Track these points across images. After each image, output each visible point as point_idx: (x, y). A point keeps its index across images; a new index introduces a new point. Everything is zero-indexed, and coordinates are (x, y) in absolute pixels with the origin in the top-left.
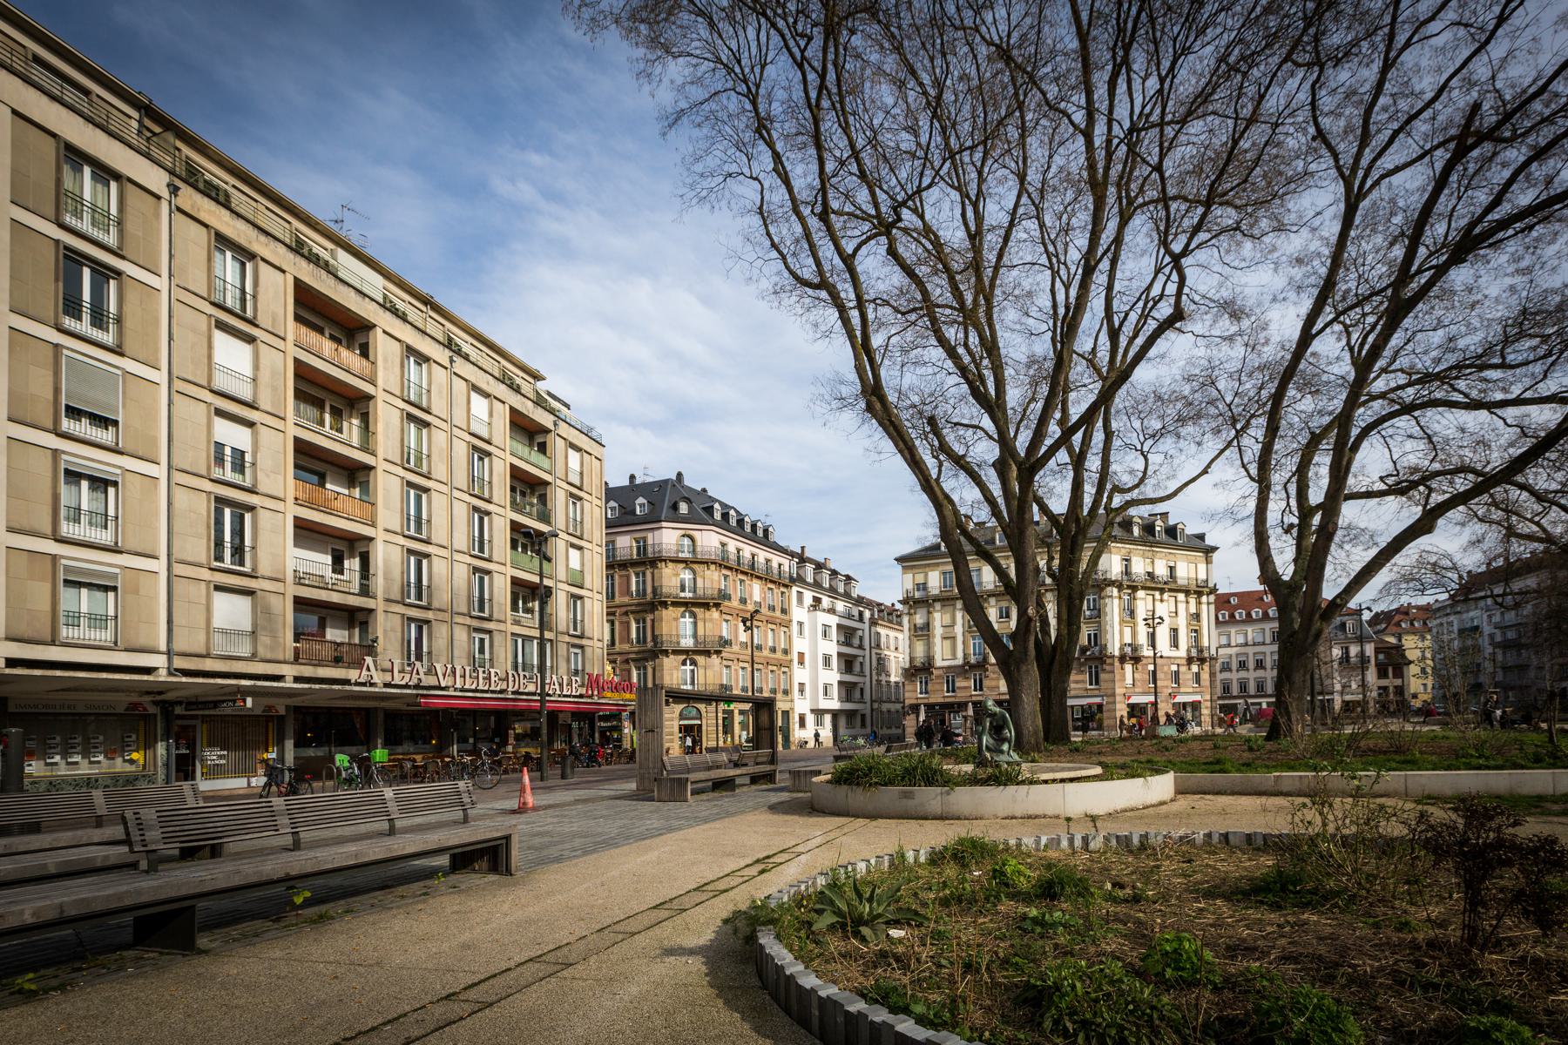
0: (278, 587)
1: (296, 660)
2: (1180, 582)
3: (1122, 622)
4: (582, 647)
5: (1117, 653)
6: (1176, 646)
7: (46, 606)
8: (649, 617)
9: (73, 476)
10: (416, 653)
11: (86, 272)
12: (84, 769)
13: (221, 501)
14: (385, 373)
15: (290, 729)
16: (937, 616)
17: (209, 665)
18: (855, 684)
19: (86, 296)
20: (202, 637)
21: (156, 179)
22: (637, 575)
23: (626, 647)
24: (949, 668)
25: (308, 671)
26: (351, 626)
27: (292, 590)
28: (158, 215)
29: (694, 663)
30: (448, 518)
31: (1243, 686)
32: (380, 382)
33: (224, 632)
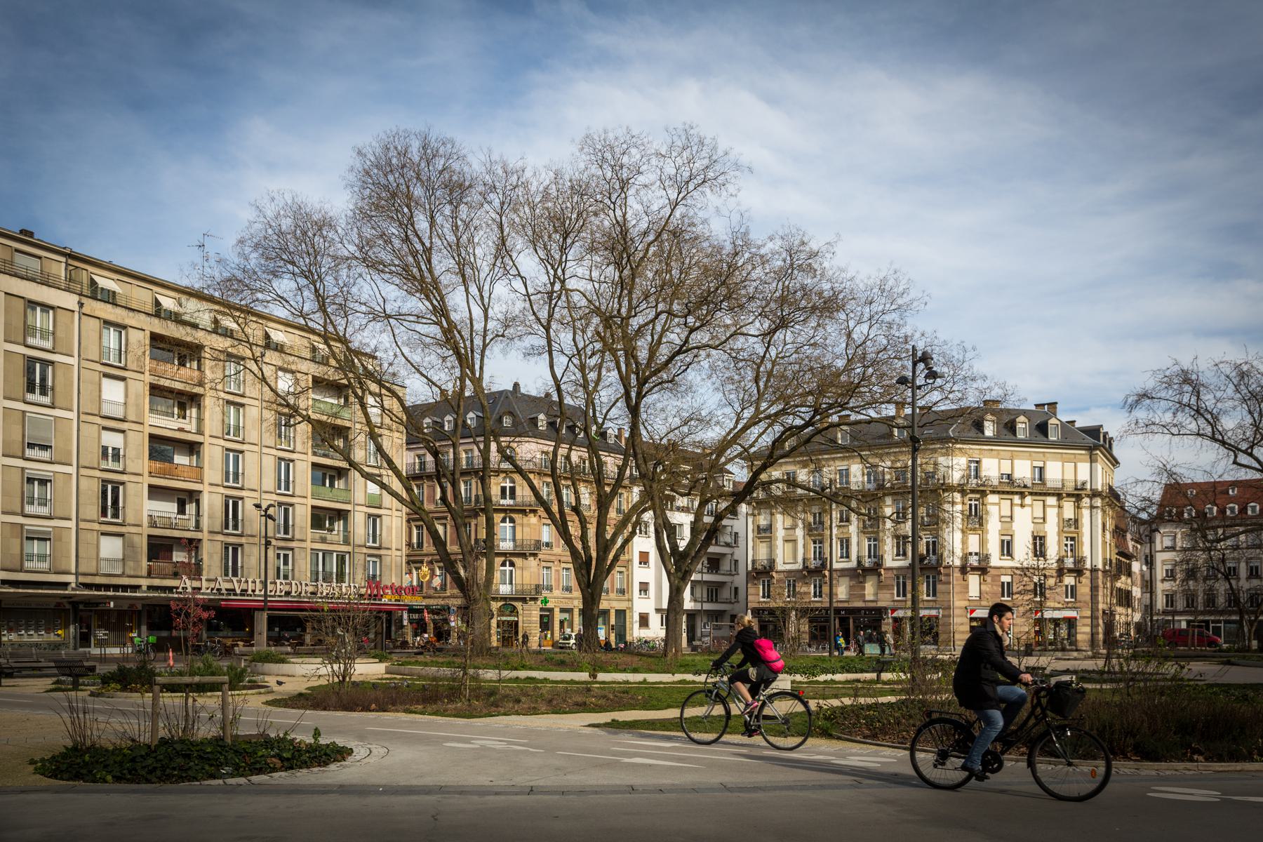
1: (149, 575)
2: (1049, 484)
4: (380, 556)
5: (958, 563)
7: (18, 551)
10: (232, 568)
12: (36, 639)
15: (144, 619)
16: (779, 517)
17: (98, 580)
18: (722, 584)
20: (94, 563)
22: (466, 483)
24: (790, 572)
25: (157, 582)
28: (73, 322)
29: (512, 564)
31: (1211, 599)
33: (107, 560)
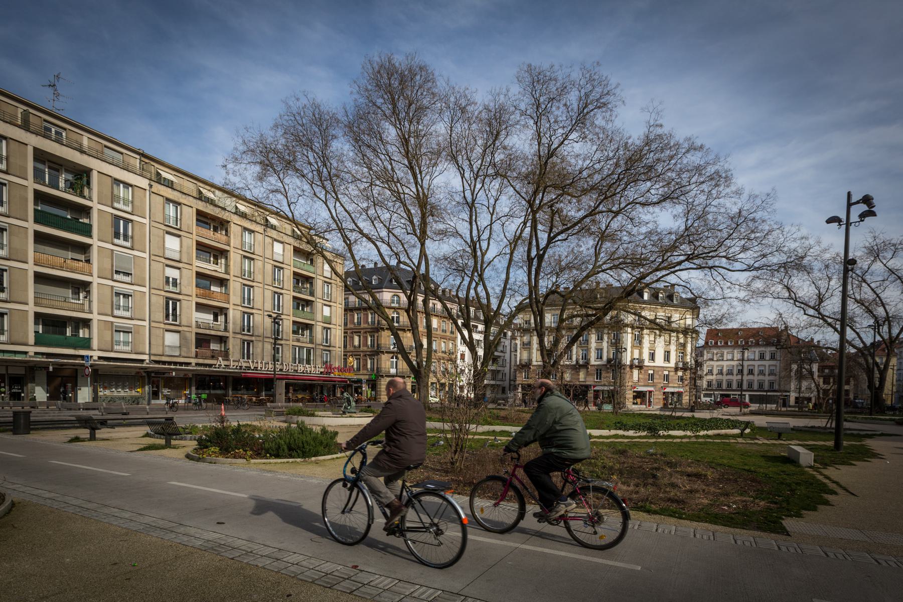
0: (189, 329)
1: (196, 357)
3: (633, 347)
5: (628, 363)
6: (668, 361)
7: (109, 339)
8: (376, 335)
9: (118, 294)
11: (122, 222)
12: (122, 394)
13: (168, 299)
14: (236, 239)
15: (194, 383)
18: (498, 371)
19: (122, 231)
21: (144, 183)
23: (365, 349)
25: (201, 361)
26: (221, 343)
27: (195, 330)
28: (145, 196)
30: (262, 298)
32: (232, 245)
33: (169, 346)
